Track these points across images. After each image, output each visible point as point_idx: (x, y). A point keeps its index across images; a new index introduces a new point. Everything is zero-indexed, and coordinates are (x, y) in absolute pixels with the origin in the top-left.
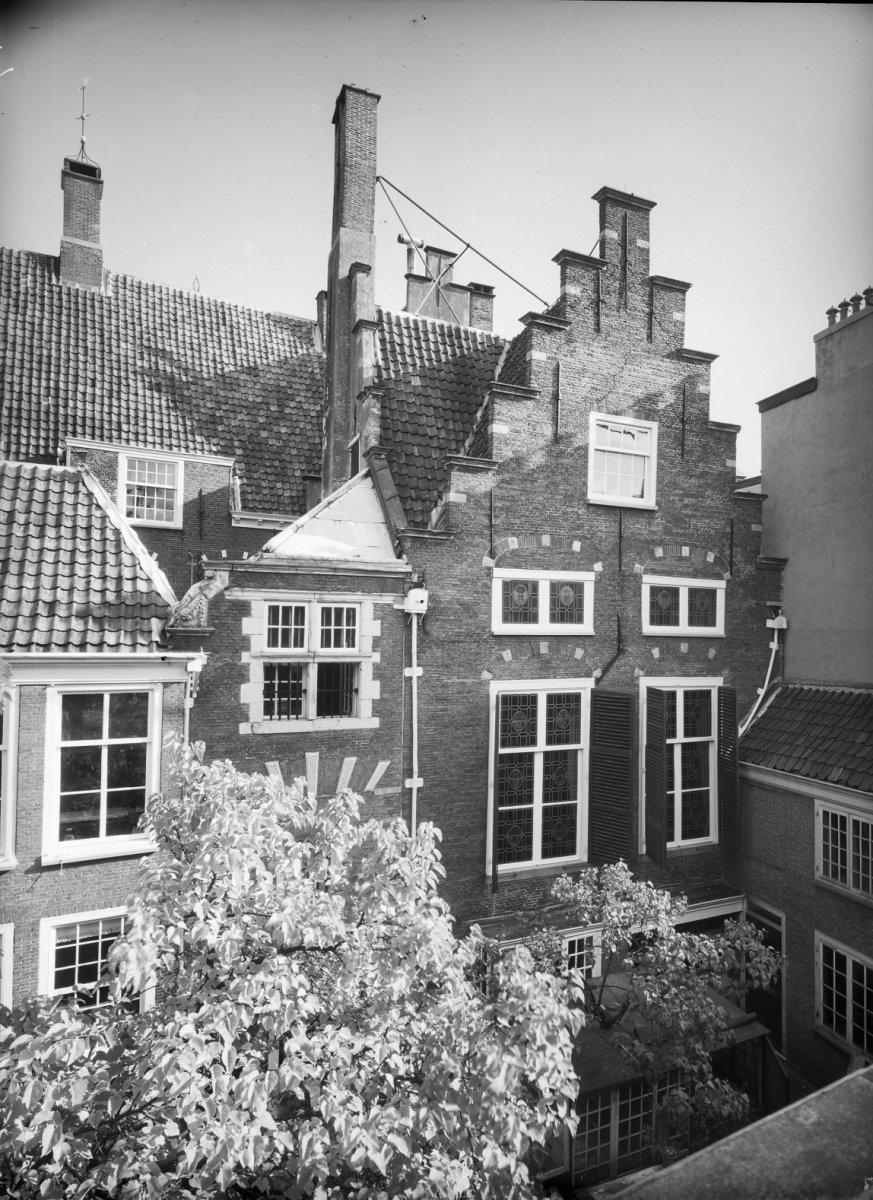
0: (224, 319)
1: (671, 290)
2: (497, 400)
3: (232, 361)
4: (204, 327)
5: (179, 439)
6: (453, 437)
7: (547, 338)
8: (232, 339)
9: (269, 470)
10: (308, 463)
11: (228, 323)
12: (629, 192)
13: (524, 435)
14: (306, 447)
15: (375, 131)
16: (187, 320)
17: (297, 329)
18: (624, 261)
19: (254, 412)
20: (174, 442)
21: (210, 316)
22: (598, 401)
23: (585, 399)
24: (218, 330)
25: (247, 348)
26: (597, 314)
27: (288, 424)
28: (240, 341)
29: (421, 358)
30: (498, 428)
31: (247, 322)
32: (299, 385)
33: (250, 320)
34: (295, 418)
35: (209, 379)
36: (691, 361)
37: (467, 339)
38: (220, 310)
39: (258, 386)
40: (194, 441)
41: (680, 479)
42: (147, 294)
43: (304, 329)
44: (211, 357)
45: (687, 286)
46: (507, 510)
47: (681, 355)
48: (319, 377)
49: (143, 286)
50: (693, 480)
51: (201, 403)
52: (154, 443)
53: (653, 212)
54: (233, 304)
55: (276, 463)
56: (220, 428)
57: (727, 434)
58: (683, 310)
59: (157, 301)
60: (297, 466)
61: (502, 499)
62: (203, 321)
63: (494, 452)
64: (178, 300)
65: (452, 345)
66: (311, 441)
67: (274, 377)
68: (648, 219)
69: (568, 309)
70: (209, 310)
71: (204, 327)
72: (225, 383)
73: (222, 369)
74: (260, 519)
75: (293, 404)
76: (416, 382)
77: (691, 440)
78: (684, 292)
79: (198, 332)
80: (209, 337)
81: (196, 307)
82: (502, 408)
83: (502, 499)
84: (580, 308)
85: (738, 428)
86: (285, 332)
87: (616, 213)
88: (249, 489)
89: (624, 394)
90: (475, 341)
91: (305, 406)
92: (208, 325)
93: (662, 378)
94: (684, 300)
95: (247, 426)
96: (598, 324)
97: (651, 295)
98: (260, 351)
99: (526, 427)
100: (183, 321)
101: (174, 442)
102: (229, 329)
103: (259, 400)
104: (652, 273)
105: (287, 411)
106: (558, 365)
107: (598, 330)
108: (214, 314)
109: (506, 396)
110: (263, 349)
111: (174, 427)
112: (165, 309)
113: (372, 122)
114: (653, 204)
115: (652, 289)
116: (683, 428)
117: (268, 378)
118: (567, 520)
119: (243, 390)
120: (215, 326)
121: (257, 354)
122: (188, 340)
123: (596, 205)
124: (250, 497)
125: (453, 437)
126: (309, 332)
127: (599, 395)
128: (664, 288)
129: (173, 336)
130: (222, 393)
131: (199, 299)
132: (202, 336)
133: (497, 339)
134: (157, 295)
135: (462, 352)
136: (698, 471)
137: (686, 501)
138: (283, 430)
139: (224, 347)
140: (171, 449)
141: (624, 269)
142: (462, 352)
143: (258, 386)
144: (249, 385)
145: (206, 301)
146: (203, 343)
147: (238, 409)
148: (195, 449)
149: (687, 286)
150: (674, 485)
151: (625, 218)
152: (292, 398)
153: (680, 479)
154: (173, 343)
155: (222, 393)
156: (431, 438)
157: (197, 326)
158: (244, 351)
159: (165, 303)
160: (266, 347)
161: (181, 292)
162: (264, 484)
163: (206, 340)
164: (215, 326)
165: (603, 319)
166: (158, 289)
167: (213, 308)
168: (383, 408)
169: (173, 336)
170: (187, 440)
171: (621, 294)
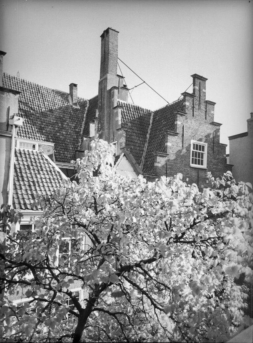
0: (39, 91)
1: (211, 104)
2: (169, 136)
3: (44, 107)
4: (33, 93)
5: (31, 135)
6: (142, 143)
7: (181, 117)
8: (43, 99)
9: (62, 147)
10: (73, 145)
11: (41, 93)
12: (201, 76)
13: (175, 146)
14: (72, 139)
15: (117, 43)
16: (27, 91)
17: (63, 96)
18: (200, 95)
19: (54, 126)
20: (30, 136)
21: (34, 90)
22: (193, 136)
23: (190, 136)
24: (38, 95)
25: (48, 102)
26: (193, 111)
27: (65, 131)
28: (45, 99)
29: (130, 116)
30: (169, 144)
31: (47, 92)
32: (67, 117)
33: (47, 92)
34: (67, 129)
35: (38, 113)
36: (215, 125)
37: (141, 111)
38: (37, 87)
39: (54, 116)
40: (36, 136)
41: (213, 160)
42: (13, 80)
43: (65, 96)
44: (37, 105)
45: (215, 103)
46: (170, 168)
47: (213, 124)
48: (72, 114)
49: (11, 77)
50: (216, 160)
51: (36, 122)
52: (24, 136)
53: (207, 81)
54: (41, 85)
55: (64, 145)
56: (44, 131)
57: (224, 146)
58: (214, 110)
59: (16, 83)
60: (70, 146)
61: (169, 165)
62: (32, 91)
63: (168, 151)
64: (23, 83)
65: (138, 113)
66: (73, 137)
67: (58, 113)
68: (205, 83)
69: (186, 109)
70: (34, 87)
71: (33, 93)
72: (43, 115)
73: (41, 110)
74: (63, 165)
75: (66, 124)
76: (129, 124)
77: (215, 148)
78: (214, 105)
79: (31, 95)
80: (35, 98)
81: (29, 86)
82: (170, 138)
83: (169, 165)
84: (189, 109)
85: (77, 85)
86: (59, 97)
87: (198, 81)
88: (57, 154)
89: (199, 135)
90: (144, 111)
91: (70, 124)
92: (34, 93)
93: (209, 130)
94: (214, 107)
95: (52, 131)
96: (193, 114)
97: (206, 106)
98: (52, 104)
99: (175, 144)
100: (26, 91)
101: (30, 136)
102: (41, 95)
103: (55, 121)
104: (206, 100)
105: (64, 126)
106: (184, 126)
107: (193, 116)
108: (35, 89)
109: (170, 135)
110: (53, 103)
111: (29, 130)
112: (19, 86)
113: (117, 40)
114: (207, 79)
115: (206, 104)
116: (214, 145)
117: (56, 114)
118: (185, 172)
119: (49, 118)
120: (36, 94)
121: (52, 105)
122: (28, 98)
123: (192, 78)
124: (57, 156)
125: (142, 143)
126: (67, 97)
127: (193, 135)
128: (209, 104)
129: (23, 96)
130: (42, 119)
131: (30, 83)
132: (33, 97)
133: (149, 111)
134: (16, 81)
135: (140, 115)
136: (217, 158)
137: (214, 166)
138: (64, 133)
139: (41, 101)
140: (29, 139)
141: (200, 98)
142: (140, 115)
143: (54, 116)
144: (51, 116)
145: (32, 84)
146: (33, 100)
147: (48, 125)
148: (37, 139)
149: (215, 103)
150: (211, 162)
151: (200, 83)
152: (65, 121)
153: (213, 160)
154: (24, 99)
155: (42, 119)
156: (136, 143)
157: (31, 93)
158: (47, 103)
159: (19, 84)
160: (54, 102)
161: (24, 80)
162: (61, 152)
163: (34, 98)
164: (36, 94)
165: (194, 112)
166: (16, 79)
167: (35, 87)
168: (126, 134)
169: (23, 96)
170: (34, 135)
171: (199, 105)
